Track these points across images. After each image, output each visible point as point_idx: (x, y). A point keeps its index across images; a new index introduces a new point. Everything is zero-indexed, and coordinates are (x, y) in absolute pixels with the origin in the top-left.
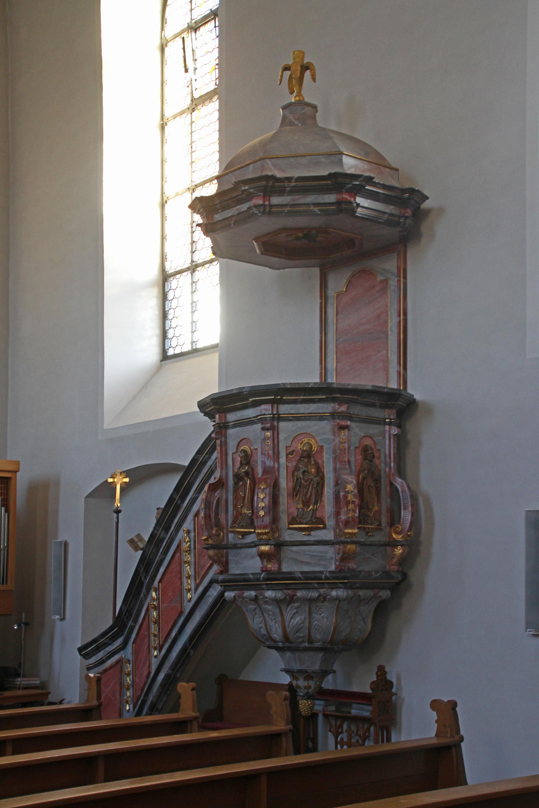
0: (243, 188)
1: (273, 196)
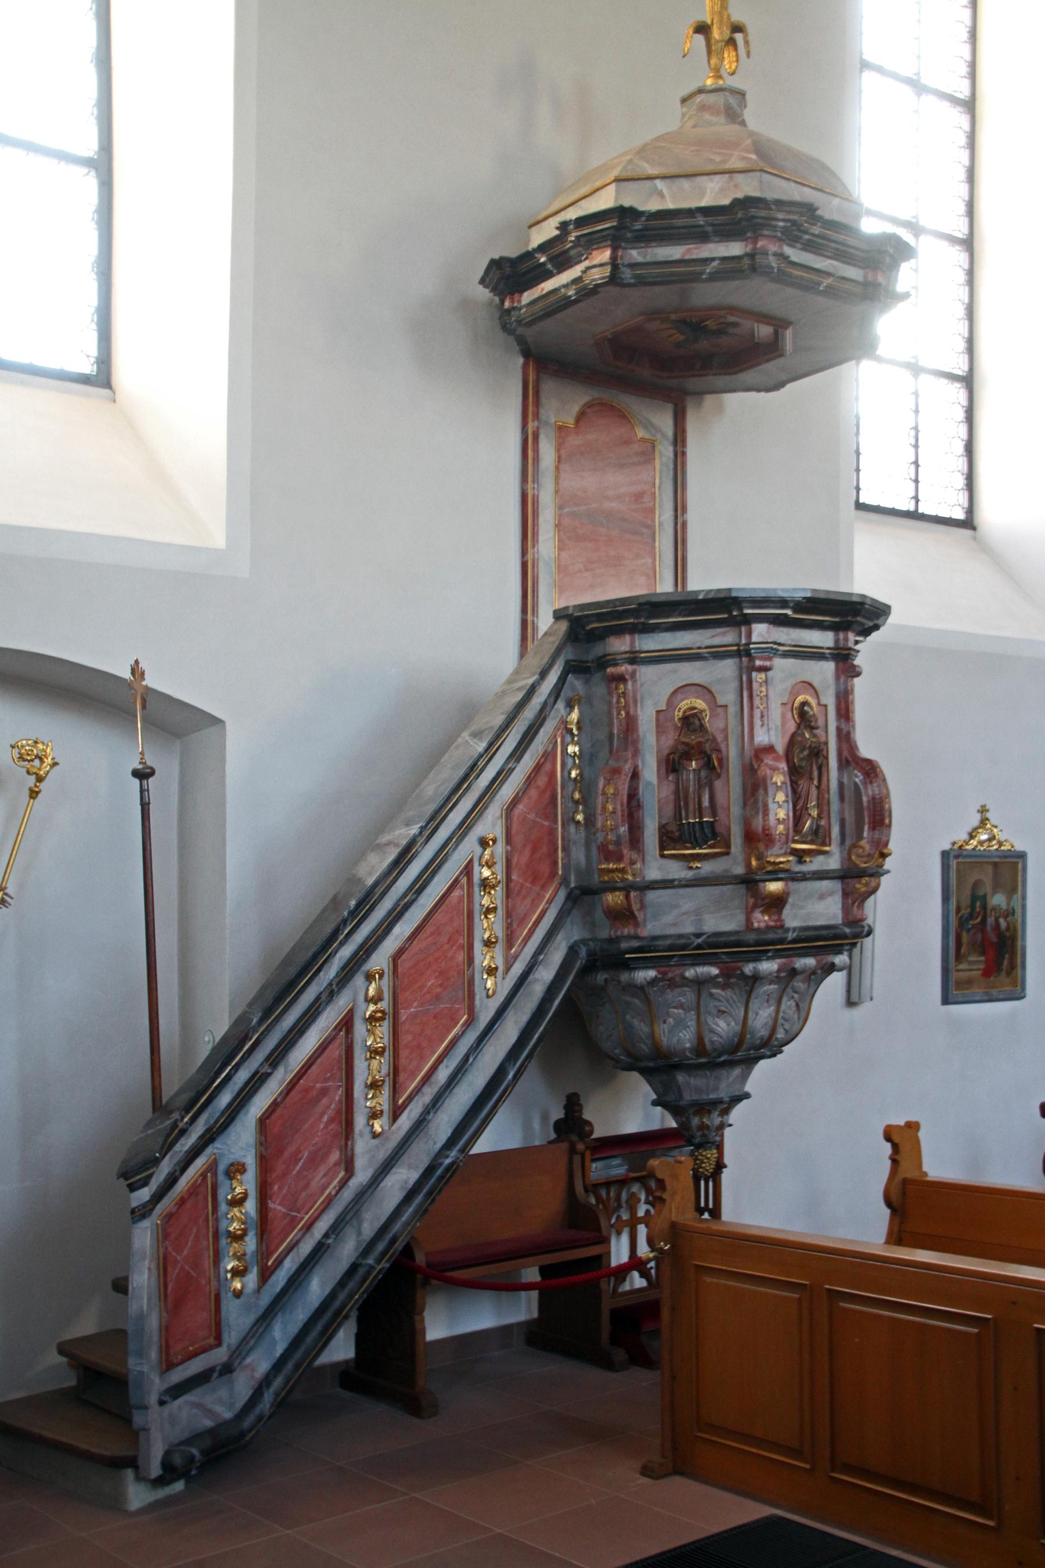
1: (895, 285)
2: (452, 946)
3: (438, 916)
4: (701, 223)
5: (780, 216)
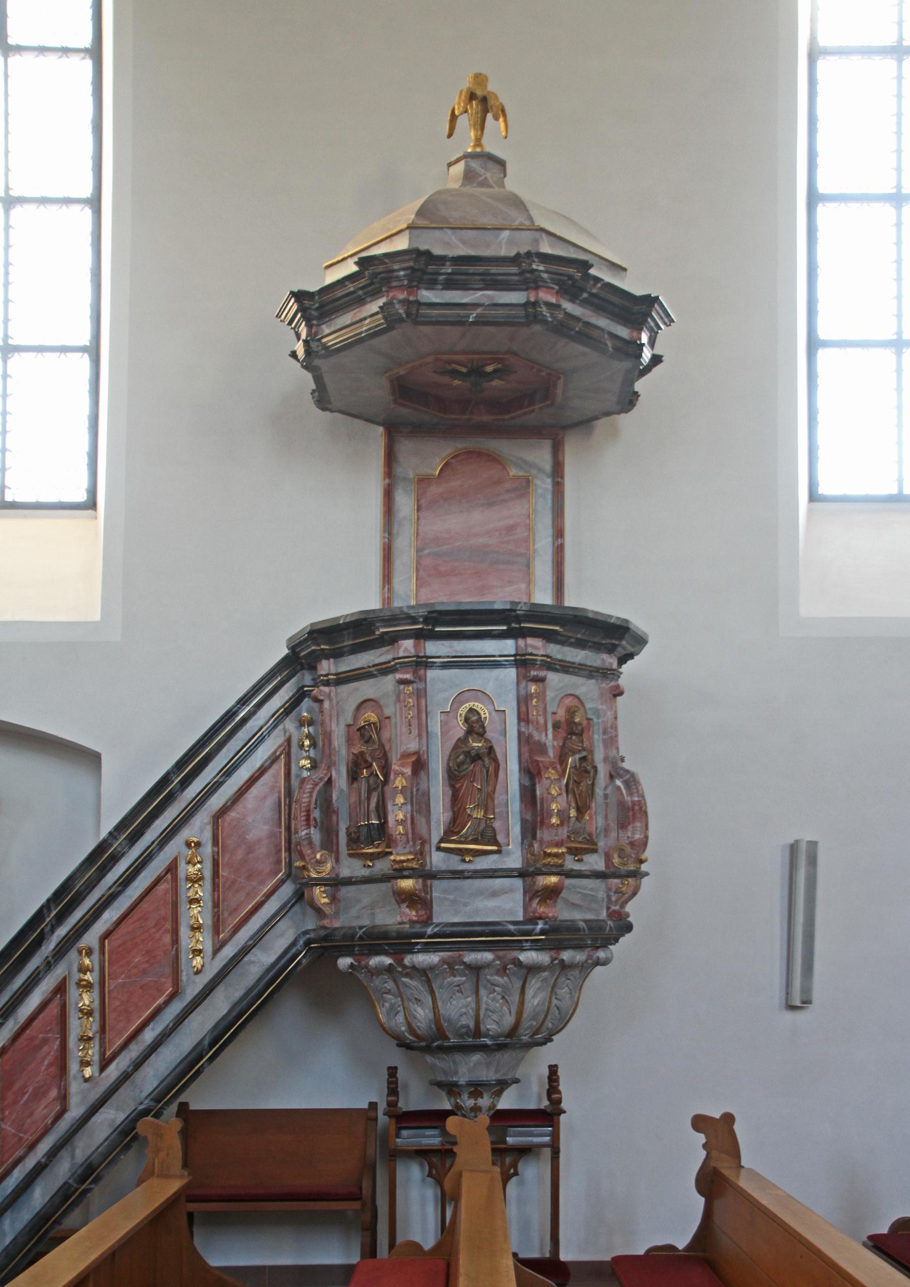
0: (534, 267)
2: (159, 929)
3: (144, 905)
4: (352, 289)
5: (396, 267)
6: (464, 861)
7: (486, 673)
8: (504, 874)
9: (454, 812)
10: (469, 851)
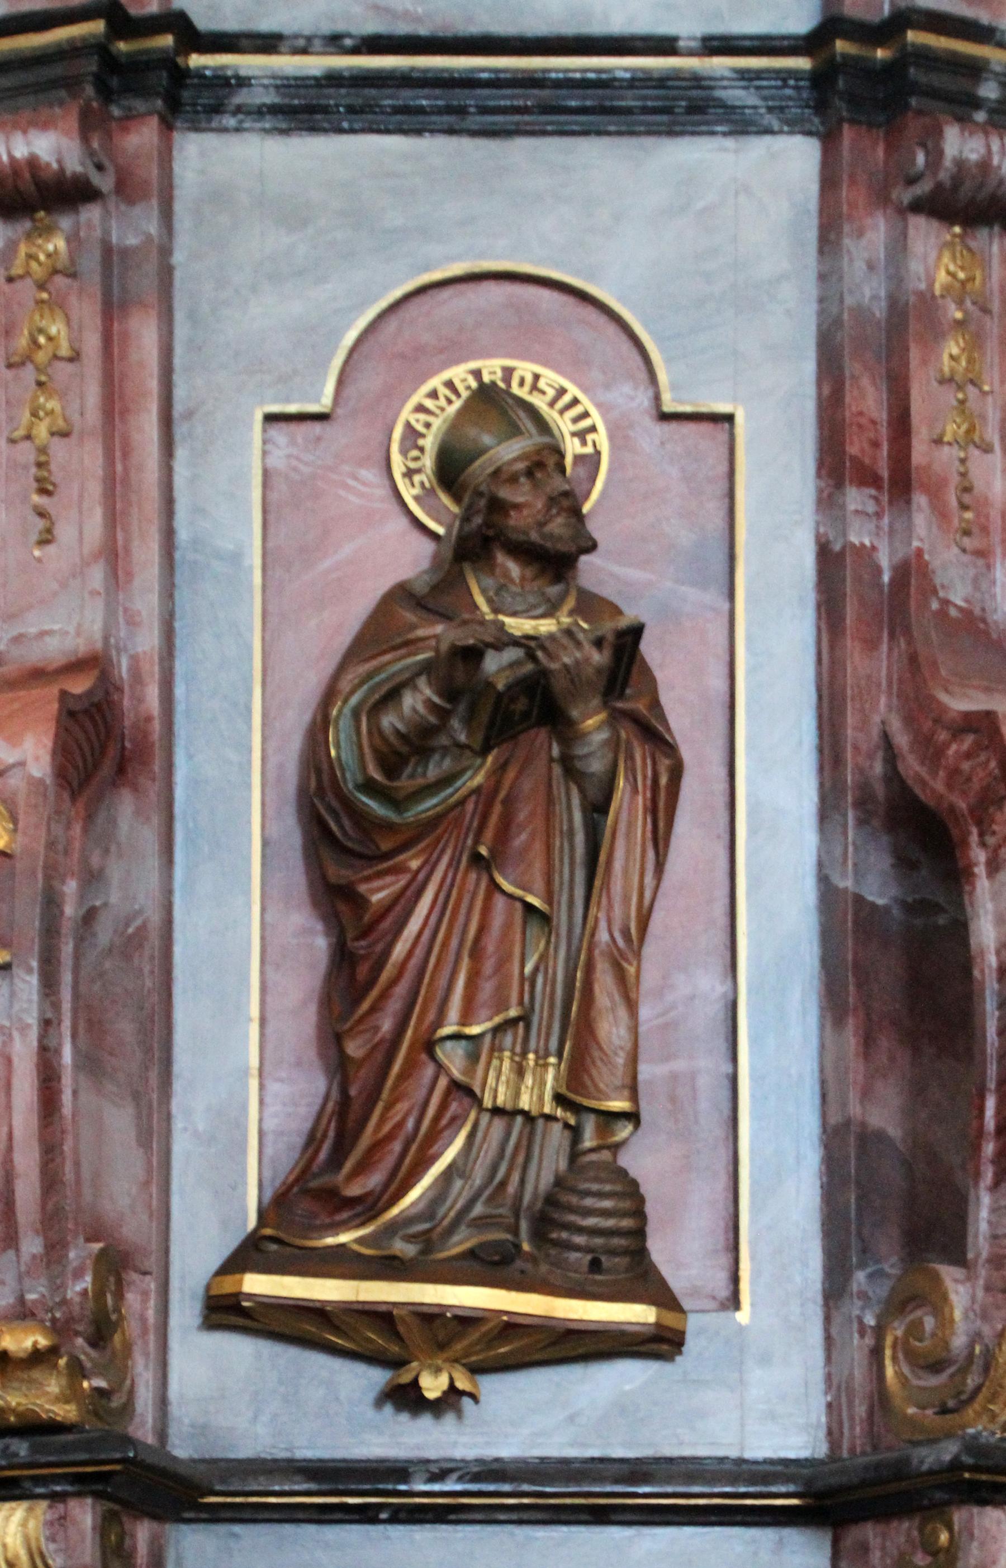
6: (406, 1398)
7: (600, 163)
8: (702, 1494)
9: (339, 1066)
10: (443, 1329)
